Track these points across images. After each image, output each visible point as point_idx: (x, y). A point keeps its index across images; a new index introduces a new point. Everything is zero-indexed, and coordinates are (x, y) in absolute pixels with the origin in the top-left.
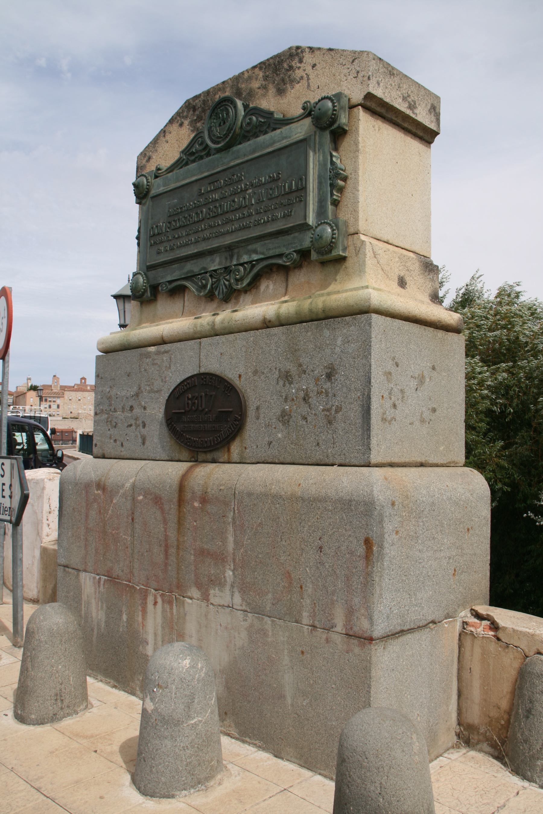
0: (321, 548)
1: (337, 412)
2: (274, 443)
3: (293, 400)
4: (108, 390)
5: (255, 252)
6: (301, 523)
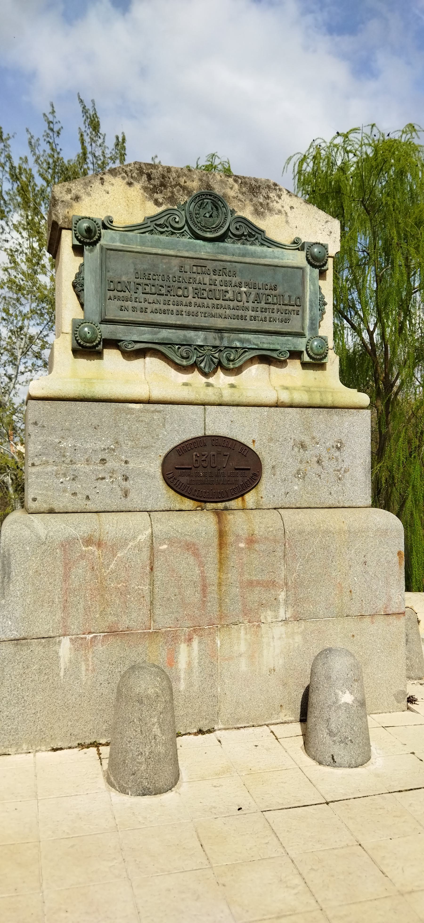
0: (365, 563)
1: (345, 472)
2: (290, 493)
3: (308, 462)
4: (57, 440)
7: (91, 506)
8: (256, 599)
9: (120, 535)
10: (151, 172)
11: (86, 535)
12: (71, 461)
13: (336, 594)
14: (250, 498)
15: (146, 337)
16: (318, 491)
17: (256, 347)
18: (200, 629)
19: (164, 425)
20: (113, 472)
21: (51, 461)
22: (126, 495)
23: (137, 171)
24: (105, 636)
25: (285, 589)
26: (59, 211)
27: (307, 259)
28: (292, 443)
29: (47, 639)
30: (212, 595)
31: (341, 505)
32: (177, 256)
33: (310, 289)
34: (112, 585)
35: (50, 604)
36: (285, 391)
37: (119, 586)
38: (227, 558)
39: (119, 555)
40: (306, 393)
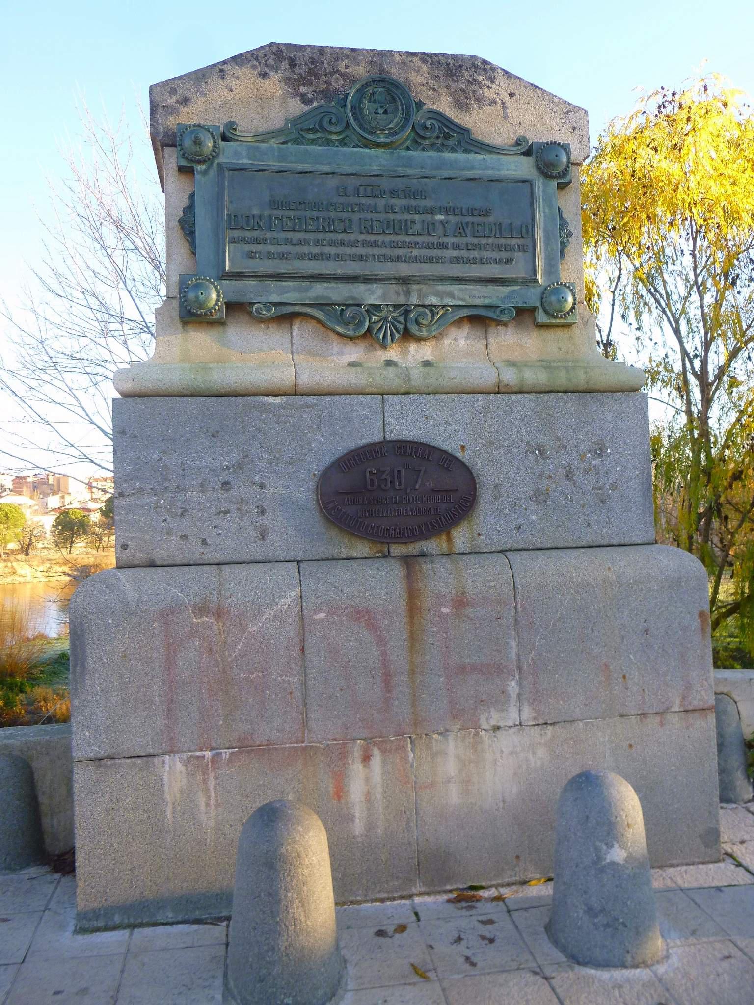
0: (647, 631)
2: (525, 526)
3: (551, 477)
5: (452, 296)
6: (618, 609)
7: (210, 555)
8: (472, 692)
9: (250, 599)
10: (294, 56)
11: (197, 599)
12: (178, 487)
13: (600, 682)
14: (461, 536)
15: (290, 297)
16: (570, 520)
17: (464, 304)
18: (384, 741)
19: (319, 427)
20: (243, 501)
21: (147, 487)
22: (263, 537)
23: (273, 57)
24: (233, 753)
25: (517, 677)
26: (160, 121)
27: (538, 168)
28: (524, 448)
29: (145, 759)
30: (401, 689)
31: (607, 542)
32: (333, 174)
33: (544, 212)
34: (242, 675)
35: (147, 705)
36: (511, 368)
37: (252, 676)
38: (423, 630)
39: (250, 630)
40: (544, 370)
